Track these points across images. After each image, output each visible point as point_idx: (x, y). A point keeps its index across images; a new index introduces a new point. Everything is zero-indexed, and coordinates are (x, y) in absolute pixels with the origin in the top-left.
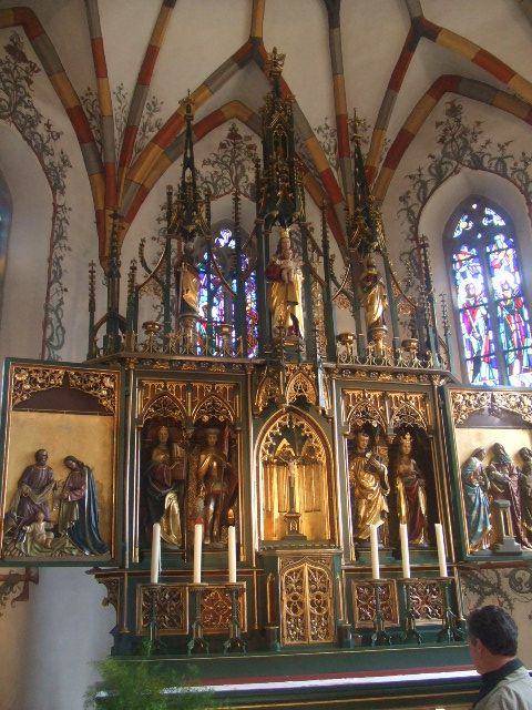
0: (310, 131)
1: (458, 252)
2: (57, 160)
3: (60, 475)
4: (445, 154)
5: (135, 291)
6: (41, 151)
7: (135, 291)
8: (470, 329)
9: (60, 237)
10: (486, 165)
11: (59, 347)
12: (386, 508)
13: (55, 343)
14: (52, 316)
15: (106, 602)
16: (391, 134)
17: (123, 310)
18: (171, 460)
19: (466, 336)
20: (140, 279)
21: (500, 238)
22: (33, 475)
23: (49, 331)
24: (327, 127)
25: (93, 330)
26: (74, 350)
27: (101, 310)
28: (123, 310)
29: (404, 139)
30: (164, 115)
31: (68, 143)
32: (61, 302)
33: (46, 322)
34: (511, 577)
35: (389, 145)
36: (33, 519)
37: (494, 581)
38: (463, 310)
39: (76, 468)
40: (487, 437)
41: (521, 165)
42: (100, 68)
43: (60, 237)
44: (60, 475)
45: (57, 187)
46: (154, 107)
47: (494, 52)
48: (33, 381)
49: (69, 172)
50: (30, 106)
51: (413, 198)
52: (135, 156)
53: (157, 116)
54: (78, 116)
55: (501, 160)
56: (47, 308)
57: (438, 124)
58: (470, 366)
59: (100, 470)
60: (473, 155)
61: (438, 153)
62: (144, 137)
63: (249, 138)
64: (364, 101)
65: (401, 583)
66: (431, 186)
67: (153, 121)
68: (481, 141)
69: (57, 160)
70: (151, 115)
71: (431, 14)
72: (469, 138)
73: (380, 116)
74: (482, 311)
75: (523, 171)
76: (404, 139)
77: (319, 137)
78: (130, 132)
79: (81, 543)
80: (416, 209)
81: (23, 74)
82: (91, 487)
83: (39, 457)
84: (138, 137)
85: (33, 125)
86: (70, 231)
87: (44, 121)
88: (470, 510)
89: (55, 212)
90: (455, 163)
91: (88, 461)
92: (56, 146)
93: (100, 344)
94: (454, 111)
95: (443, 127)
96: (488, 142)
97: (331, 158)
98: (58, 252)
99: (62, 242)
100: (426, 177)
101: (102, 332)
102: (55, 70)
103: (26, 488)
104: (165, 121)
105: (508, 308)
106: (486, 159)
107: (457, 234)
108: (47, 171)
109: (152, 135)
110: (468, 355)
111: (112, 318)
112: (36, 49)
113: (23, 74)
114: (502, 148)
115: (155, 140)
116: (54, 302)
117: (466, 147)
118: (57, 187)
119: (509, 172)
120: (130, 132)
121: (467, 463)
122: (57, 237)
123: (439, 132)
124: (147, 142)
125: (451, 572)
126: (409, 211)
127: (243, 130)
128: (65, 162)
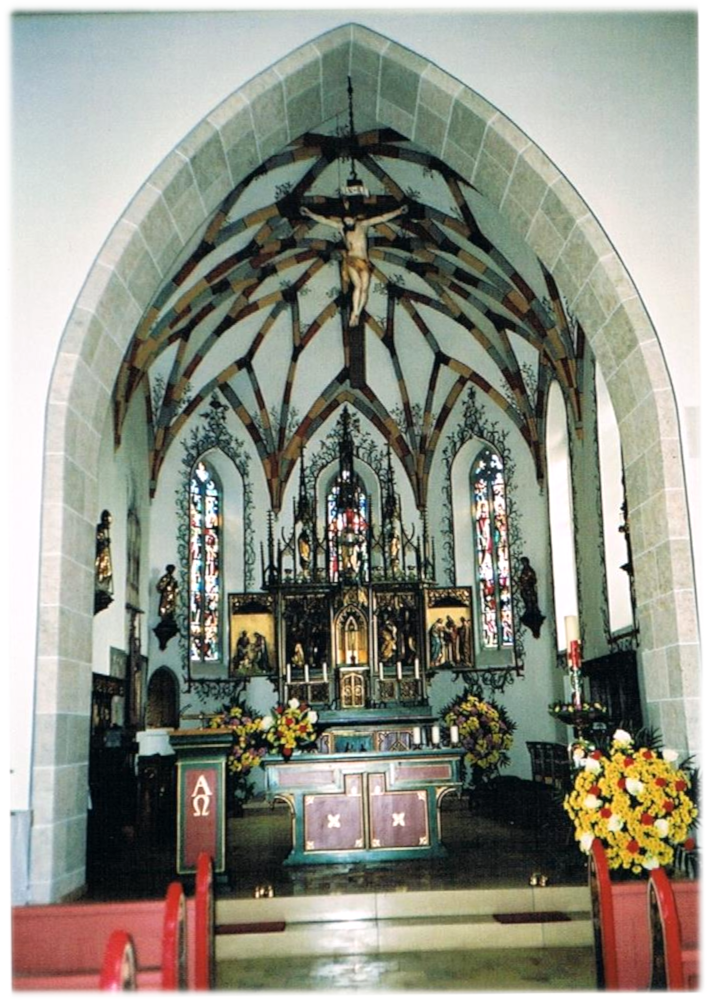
0: (387, 414)
1: (478, 482)
2: (243, 458)
3: (253, 640)
4: (466, 425)
5: (280, 553)
6: (233, 457)
7: (280, 553)
8: (481, 532)
9: (249, 502)
10: (485, 435)
11: (252, 564)
12: (394, 647)
13: (250, 562)
14: (248, 548)
15: (274, 691)
16: (436, 409)
17: (276, 564)
18: (298, 630)
19: (479, 536)
20: (282, 547)
21: (499, 476)
22: (243, 641)
23: (247, 556)
24: (398, 409)
25: (264, 572)
26: (256, 587)
27: (267, 563)
28: (276, 564)
29: (446, 411)
30: (300, 418)
31: (249, 447)
32: (252, 539)
33: (245, 552)
34: (483, 676)
35: (437, 417)
36: (243, 659)
37: (476, 678)
38: (478, 521)
39: (259, 637)
40: (443, 613)
41: (501, 439)
42: (261, 404)
43: (249, 502)
44: (253, 640)
45: (244, 473)
46: (294, 414)
47: (478, 372)
48: (239, 602)
49: (250, 462)
50: (226, 434)
51: (449, 453)
52: (286, 443)
53: (296, 418)
54: (252, 428)
55: (492, 433)
56: (245, 544)
57: (464, 403)
58: (480, 555)
59: (270, 640)
60: (479, 428)
61: (462, 424)
62: (290, 431)
63: (354, 415)
64: (418, 397)
65: (399, 681)
66: (458, 445)
67: (294, 422)
68: (483, 420)
69: (243, 458)
70: (292, 418)
71: (446, 350)
72: (478, 416)
73: (427, 404)
74: (488, 522)
75: (502, 443)
76: (446, 411)
77: (394, 416)
78: (282, 431)
79: (262, 668)
80: (450, 460)
81: (220, 415)
82: (265, 644)
83: (244, 634)
84: (287, 431)
85: (229, 444)
86: (254, 497)
87: (234, 439)
88: (431, 646)
89: (245, 489)
90: (470, 432)
91: (262, 632)
92: (241, 451)
93: (267, 579)
94: (472, 395)
95: (465, 406)
96: (487, 421)
97: (402, 427)
98: (248, 511)
99: (250, 505)
100: (456, 439)
101: (268, 573)
102: (237, 404)
103: (240, 646)
104: (301, 421)
105: (501, 521)
106: (485, 432)
107: (478, 471)
108: (238, 467)
109: (294, 430)
110: (480, 548)
111: (271, 566)
112: (226, 397)
113: (220, 415)
114: (493, 425)
115: (297, 433)
116: (248, 541)
117: (476, 423)
118: (244, 473)
119: (496, 442)
120: (282, 431)
121: (433, 626)
122: (247, 503)
123: (464, 408)
124: (292, 434)
125: (421, 676)
126: (448, 462)
127: (352, 409)
128: (248, 457)
